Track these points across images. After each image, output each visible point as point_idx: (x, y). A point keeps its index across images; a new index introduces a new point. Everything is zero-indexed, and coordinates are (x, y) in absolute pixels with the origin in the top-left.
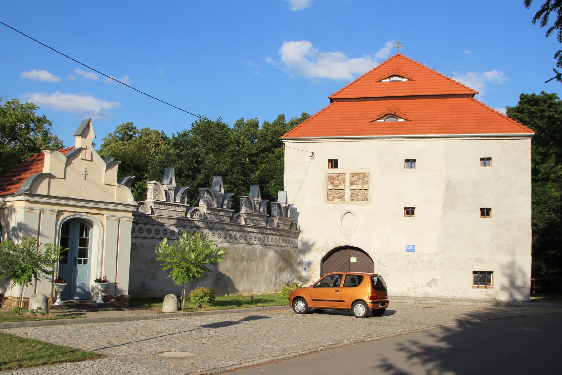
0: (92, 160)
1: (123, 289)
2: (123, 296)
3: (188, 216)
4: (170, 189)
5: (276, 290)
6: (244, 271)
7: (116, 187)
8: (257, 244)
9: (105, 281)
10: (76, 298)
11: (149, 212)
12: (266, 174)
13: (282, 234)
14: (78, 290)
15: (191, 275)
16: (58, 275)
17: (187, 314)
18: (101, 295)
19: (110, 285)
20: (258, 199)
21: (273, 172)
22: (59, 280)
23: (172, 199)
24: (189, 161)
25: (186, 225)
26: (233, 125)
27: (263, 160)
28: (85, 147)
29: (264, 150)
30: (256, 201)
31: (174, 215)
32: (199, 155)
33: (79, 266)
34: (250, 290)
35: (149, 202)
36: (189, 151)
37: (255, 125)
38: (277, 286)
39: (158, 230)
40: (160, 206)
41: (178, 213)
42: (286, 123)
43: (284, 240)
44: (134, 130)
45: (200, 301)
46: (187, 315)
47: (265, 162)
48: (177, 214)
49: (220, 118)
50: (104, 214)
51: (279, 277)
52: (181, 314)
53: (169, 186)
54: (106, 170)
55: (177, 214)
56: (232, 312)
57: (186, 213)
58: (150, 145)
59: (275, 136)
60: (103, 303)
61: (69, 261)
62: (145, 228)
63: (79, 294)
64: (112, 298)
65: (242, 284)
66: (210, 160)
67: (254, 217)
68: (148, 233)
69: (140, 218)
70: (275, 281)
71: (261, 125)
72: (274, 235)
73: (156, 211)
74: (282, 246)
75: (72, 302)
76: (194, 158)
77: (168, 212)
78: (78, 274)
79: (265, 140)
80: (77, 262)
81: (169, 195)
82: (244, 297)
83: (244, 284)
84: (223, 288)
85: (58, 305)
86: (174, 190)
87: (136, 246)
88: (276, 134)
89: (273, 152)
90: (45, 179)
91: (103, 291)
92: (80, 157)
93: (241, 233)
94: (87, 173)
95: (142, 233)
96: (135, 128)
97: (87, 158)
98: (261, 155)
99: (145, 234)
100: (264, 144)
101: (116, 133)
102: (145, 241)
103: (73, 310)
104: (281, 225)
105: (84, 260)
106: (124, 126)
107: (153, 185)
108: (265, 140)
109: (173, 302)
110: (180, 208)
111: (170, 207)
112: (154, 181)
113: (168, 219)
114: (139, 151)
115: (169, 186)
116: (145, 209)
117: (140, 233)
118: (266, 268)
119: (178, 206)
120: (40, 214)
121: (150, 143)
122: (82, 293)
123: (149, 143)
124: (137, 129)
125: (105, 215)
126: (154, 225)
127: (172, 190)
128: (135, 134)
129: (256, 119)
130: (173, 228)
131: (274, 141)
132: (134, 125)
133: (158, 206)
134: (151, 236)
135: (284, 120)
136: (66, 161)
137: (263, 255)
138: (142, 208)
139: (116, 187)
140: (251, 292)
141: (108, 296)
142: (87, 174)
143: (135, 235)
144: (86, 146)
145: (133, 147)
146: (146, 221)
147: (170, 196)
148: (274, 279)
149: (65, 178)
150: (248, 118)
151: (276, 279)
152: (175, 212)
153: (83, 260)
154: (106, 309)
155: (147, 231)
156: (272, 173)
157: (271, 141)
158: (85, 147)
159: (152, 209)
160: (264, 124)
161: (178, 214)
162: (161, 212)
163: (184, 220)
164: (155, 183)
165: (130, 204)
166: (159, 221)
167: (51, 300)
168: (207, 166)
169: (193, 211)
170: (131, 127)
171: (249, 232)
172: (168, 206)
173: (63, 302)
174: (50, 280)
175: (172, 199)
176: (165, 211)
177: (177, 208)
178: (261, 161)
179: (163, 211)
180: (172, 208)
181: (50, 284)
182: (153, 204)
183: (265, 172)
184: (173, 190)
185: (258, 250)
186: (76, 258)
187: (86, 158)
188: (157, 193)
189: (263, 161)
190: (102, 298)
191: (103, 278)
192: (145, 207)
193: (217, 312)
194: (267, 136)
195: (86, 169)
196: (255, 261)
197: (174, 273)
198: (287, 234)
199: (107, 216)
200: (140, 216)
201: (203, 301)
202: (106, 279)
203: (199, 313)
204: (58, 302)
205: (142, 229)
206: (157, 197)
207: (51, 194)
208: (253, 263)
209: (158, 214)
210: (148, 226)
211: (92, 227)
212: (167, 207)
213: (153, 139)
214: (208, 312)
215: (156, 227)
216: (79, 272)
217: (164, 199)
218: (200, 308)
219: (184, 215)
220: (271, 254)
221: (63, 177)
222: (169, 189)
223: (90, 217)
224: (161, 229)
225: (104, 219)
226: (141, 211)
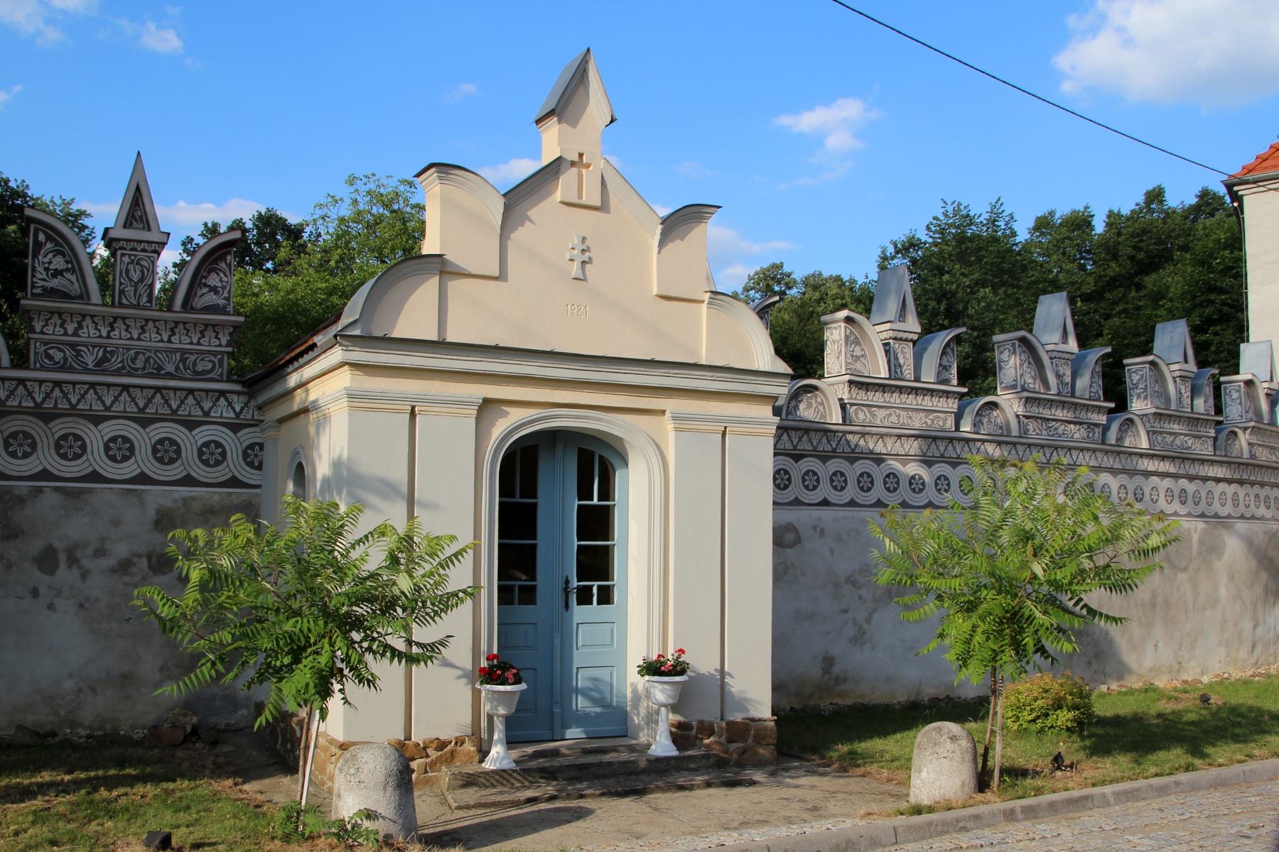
0: (603, 207)
1: (750, 695)
2: (753, 720)
3: (966, 427)
4: (901, 339)
5: (1256, 663)
6: (1154, 605)
7: (704, 306)
8: (1176, 514)
9: (679, 669)
10: (574, 733)
11: (836, 417)
12: (1126, 342)
13: (1266, 479)
14: (581, 703)
15: (1029, 641)
16: (495, 651)
17: (1018, 810)
18: (667, 719)
19: (699, 679)
20: (1185, 367)
21: (1144, 335)
22: (493, 673)
23: (908, 372)
24: (927, 311)
25: (958, 458)
26: (1027, 231)
27: (1113, 309)
28: (576, 158)
29: (1113, 283)
30: (1178, 373)
31: (917, 425)
32: (953, 294)
33: (580, 613)
34: (1176, 666)
35: (833, 385)
36: (927, 286)
37: (1080, 222)
38: (1258, 650)
39: (869, 475)
40: (871, 394)
41: (931, 417)
42: (1169, 208)
43: (1262, 498)
44: (787, 279)
45: (1039, 726)
46: (1019, 815)
47: (1120, 313)
48: (929, 422)
49: (1000, 203)
50: (663, 412)
51: (1265, 621)
52: (993, 814)
53: (894, 326)
54: (662, 244)
55: (929, 422)
56: (1194, 788)
57: (958, 417)
58: (825, 307)
59: (1142, 245)
60: (672, 751)
61: (540, 595)
62: (825, 470)
63: (582, 719)
64: (711, 733)
65: (1150, 649)
66: (983, 304)
67: (1166, 425)
68: (835, 488)
69: (805, 438)
70: (1254, 634)
71: (1099, 226)
72: (1229, 481)
73: (857, 413)
74: (1257, 519)
75: (555, 753)
76: (939, 302)
77: (899, 416)
78: (580, 644)
79: (1115, 257)
80: (574, 598)
81: (896, 358)
82: (1161, 694)
83: (1156, 646)
84: (1089, 663)
85: (492, 768)
86: (914, 343)
87: (797, 531)
88: (1145, 238)
89: (1139, 287)
90: (430, 278)
91: (674, 708)
92: (558, 196)
93: (1123, 478)
94: (587, 254)
95: (815, 488)
96: (789, 275)
97: (585, 201)
98: (1108, 296)
99: (824, 491)
100: (1114, 269)
101: (748, 291)
102: (827, 514)
103: (550, 789)
104: (1260, 449)
105: (599, 587)
106: (764, 274)
107: (843, 325)
108: (1115, 257)
109: (957, 757)
110: (935, 400)
111: (904, 397)
112: (844, 313)
113: (899, 436)
114: (800, 322)
115: (894, 326)
116: (821, 408)
117: (807, 487)
118: (1223, 592)
119: (931, 392)
120: (413, 414)
121: (825, 303)
122: (597, 713)
123: (822, 304)
124: (793, 276)
125: (668, 414)
126: (852, 460)
127: (906, 340)
128: (790, 288)
129: (1086, 208)
130: (913, 469)
131: (1141, 255)
132: (786, 269)
133: (862, 397)
134: (846, 496)
135: (1161, 202)
136: (502, 211)
137: (1211, 549)
138: (810, 406)
139: (704, 306)
140: (1178, 671)
141: (695, 724)
142: (590, 258)
143: (789, 495)
144: (581, 155)
145: (786, 317)
146: (825, 446)
147: (901, 361)
148: (1247, 625)
149: (502, 277)
150: (1063, 208)
151: (1255, 627)
152: (922, 415)
153: (595, 590)
154: (681, 781)
155: (832, 481)
156: (1142, 339)
157: (1132, 258)
158: (576, 158)
159: (843, 407)
160: (1108, 217)
161: (932, 421)
162: (874, 416)
163: (951, 440)
164: (849, 320)
165: (762, 369)
166: (871, 446)
167: (473, 749)
168: (977, 319)
169: (979, 409)
170: (781, 274)
171: (1147, 474)
172: (896, 395)
173: (515, 753)
174: (459, 672)
175: (908, 372)
176: (888, 412)
177: (927, 402)
178: (1108, 312)
179: (881, 414)
180: (911, 400)
181: (463, 692)
182: (846, 389)
183: (1124, 338)
184: (911, 340)
185: (1192, 531)
186: (567, 582)
187: (580, 197)
188: (858, 352)
189: (1114, 312)
190: (671, 733)
191: (670, 655)
192: (819, 400)
193: (1138, 790)
194: (1120, 248)
195: (584, 239)
196: (1186, 569)
197: (954, 632)
198: (1259, 479)
199: (674, 418)
200: (807, 431)
201: (1052, 727)
202: (684, 658)
203: (1070, 802)
204: (498, 758)
205: (815, 473)
206: (858, 366)
207: (451, 338)
208: (1181, 576)
209: (864, 420)
210: (835, 465)
211: (625, 463)
212: (895, 399)
213: (830, 293)
214: (1104, 795)
215: (860, 467)
216: (583, 636)
217: (884, 373)
218: (1059, 768)
219: (950, 423)
220: (1233, 547)
221: (497, 274)
222: (895, 339)
223: (609, 422)
224: (878, 473)
225: (667, 430)
226: (806, 414)
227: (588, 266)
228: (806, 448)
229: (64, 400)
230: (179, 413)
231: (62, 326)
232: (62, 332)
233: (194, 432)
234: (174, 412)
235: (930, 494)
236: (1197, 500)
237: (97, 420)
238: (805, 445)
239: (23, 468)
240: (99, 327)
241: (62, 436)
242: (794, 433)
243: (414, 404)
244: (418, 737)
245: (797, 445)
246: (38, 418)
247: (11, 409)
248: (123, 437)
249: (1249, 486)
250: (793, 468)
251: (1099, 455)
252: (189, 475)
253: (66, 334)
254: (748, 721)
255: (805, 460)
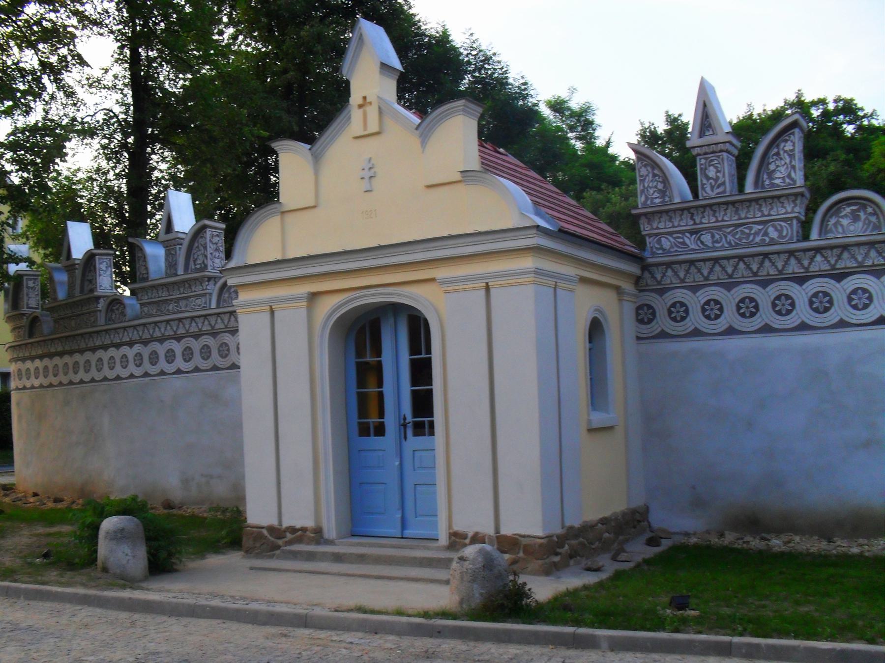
80: (410, 432)
94: (372, 171)
102: (734, 344)
198: (67, 348)
223: (399, 295)
227: (373, 180)
228: (876, 263)
229: (723, 272)
230: (734, 277)
231: (692, 218)
232: (692, 222)
233: (698, 294)
234: (755, 274)
235: (696, 319)
236: (124, 360)
237: (801, 280)
238: (846, 262)
239: (863, 317)
240: (785, 206)
241: (865, 289)
242: (829, 252)
243: (270, 304)
244: (286, 524)
245: (188, 330)
246: (721, 287)
247: (814, 274)
248: (715, 301)
249: (90, 353)
250: (834, 289)
251: (140, 329)
252: (663, 330)
253: (695, 224)
254: (517, 537)
255: (203, 337)
